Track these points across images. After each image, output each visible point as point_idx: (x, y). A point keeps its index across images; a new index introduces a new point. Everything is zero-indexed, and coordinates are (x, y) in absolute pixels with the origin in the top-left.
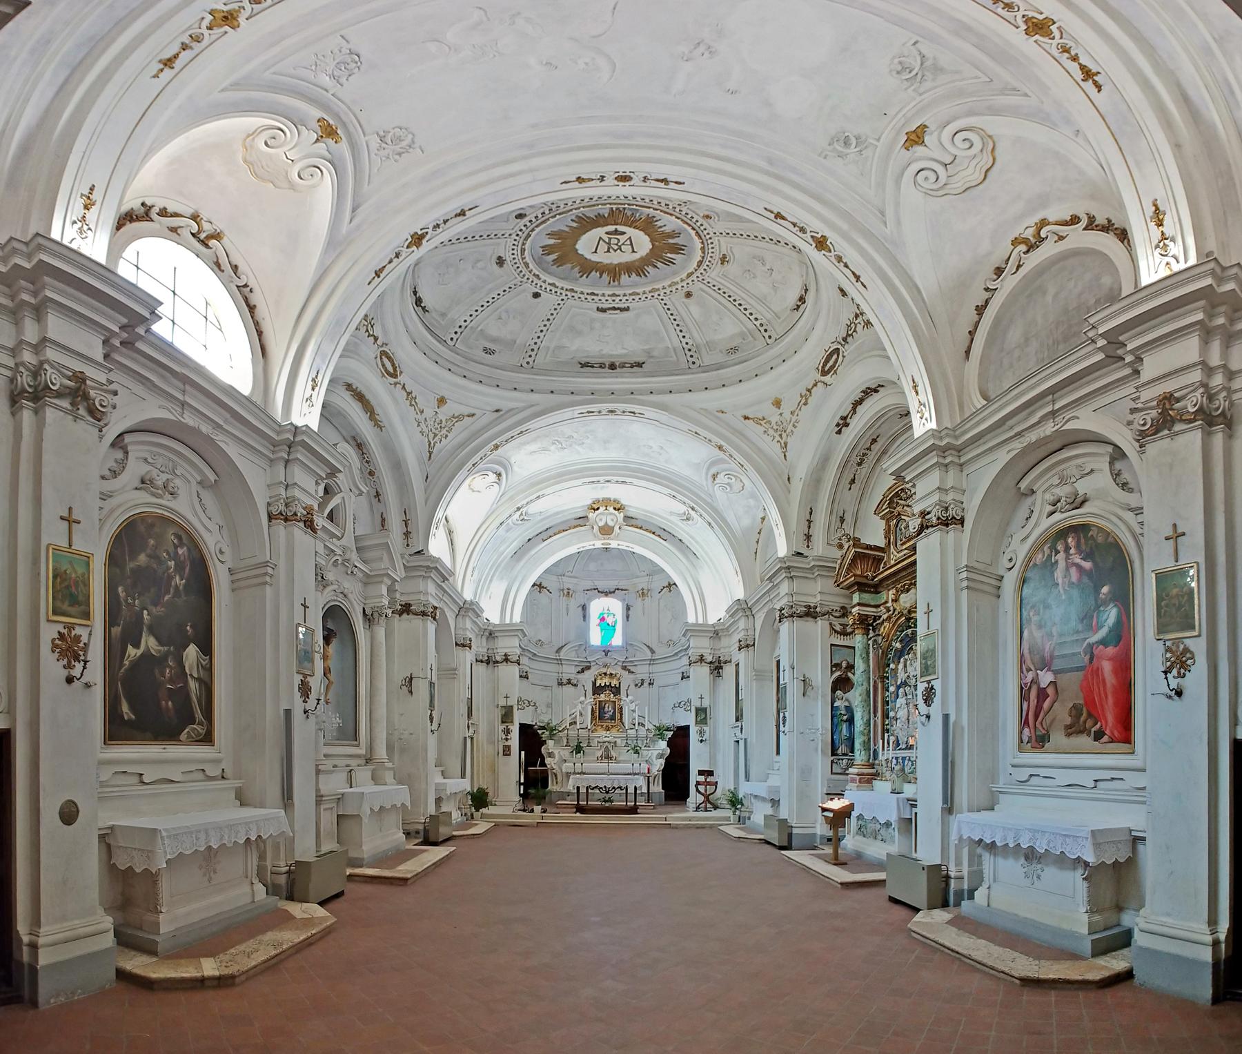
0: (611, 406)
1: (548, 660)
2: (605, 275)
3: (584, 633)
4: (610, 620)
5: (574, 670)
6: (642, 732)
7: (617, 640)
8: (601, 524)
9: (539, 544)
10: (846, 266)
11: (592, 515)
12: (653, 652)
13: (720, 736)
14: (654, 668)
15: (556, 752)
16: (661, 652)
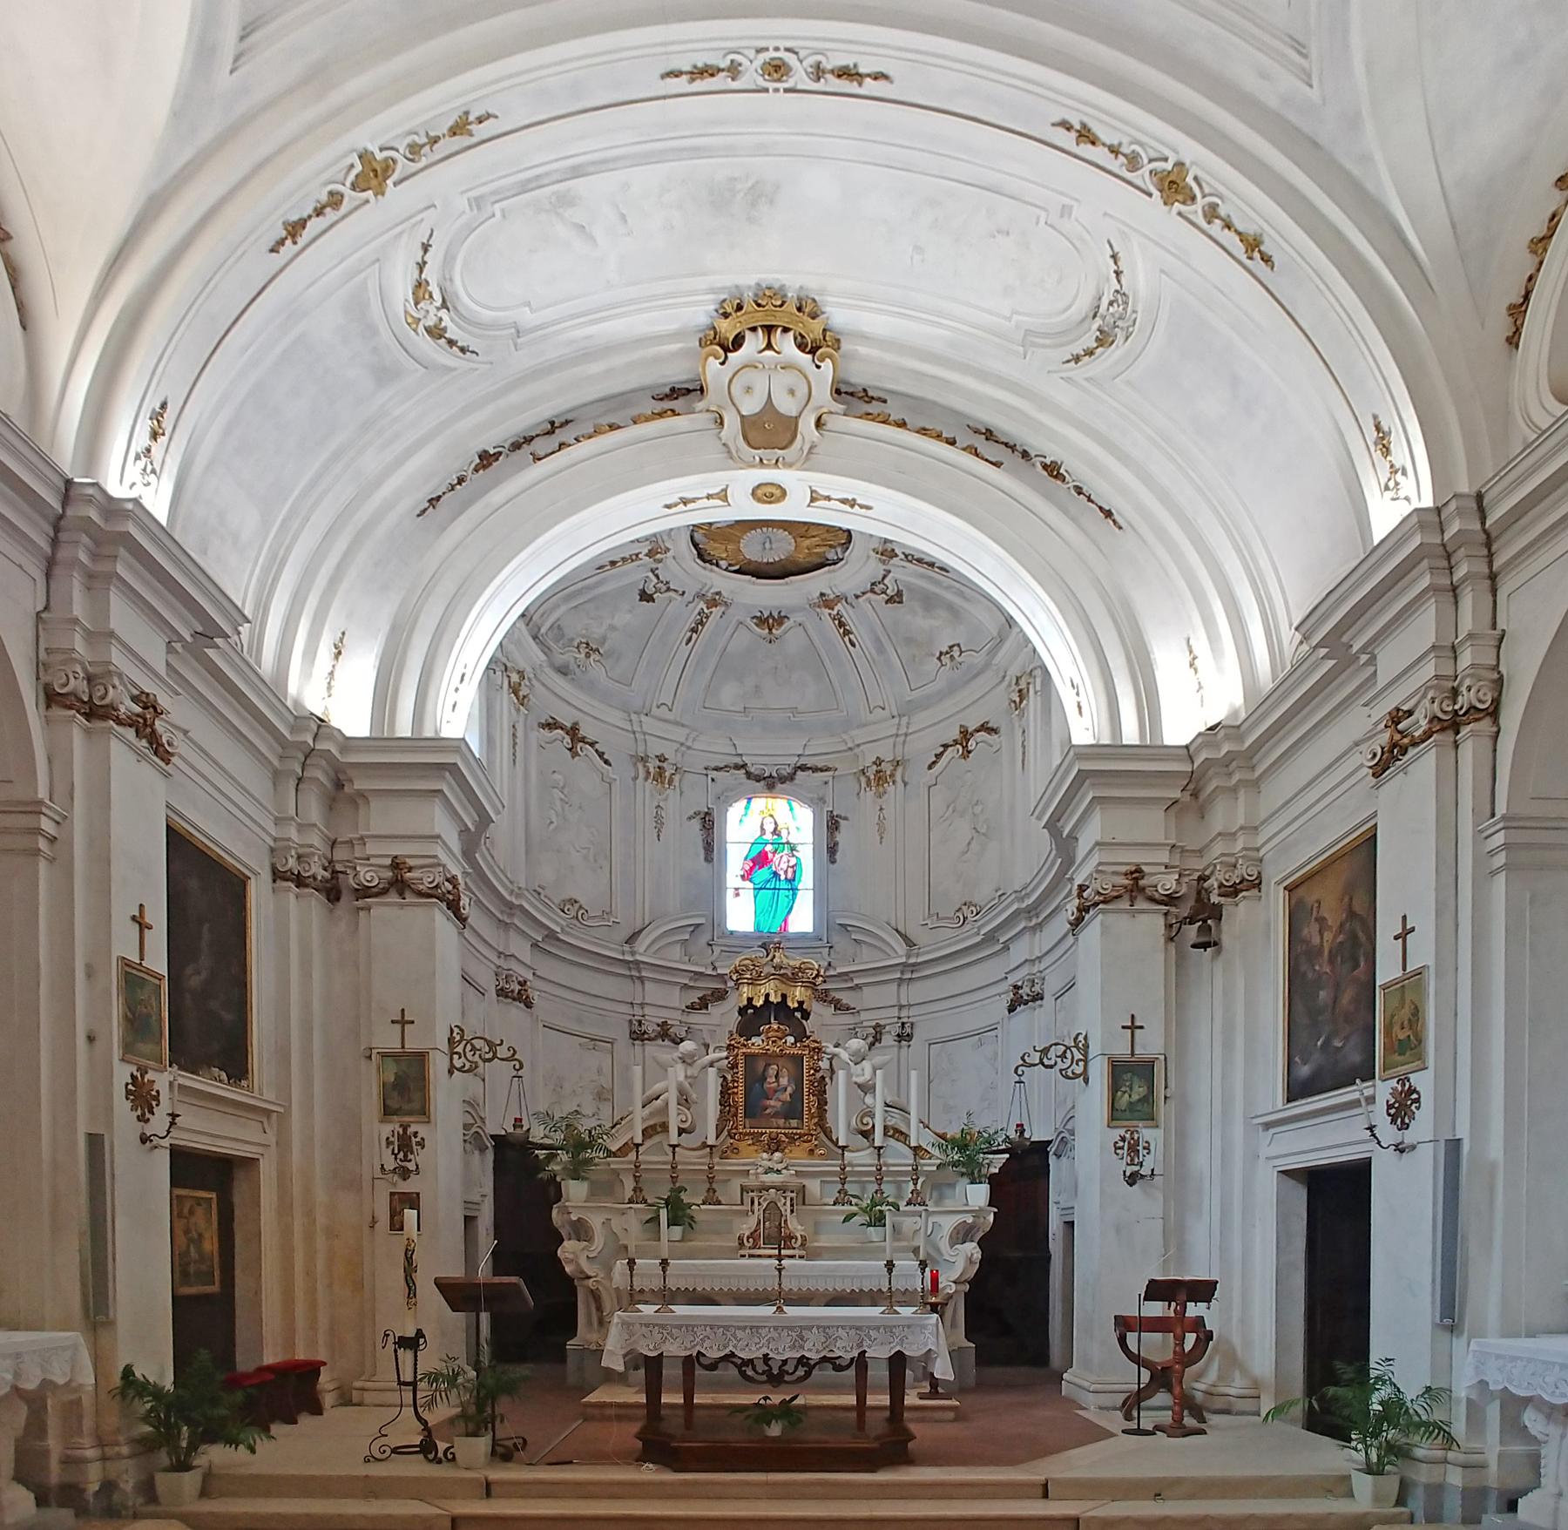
1: (602, 964)
3: (712, 896)
4: (781, 862)
5: (677, 999)
6: (898, 1157)
7: (802, 920)
8: (751, 406)
9: (521, 468)
11: (714, 371)
12: (910, 943)
13: (1201, 1157)
14: (915, 993)
15: (595, 1221)
16: (933, 944)
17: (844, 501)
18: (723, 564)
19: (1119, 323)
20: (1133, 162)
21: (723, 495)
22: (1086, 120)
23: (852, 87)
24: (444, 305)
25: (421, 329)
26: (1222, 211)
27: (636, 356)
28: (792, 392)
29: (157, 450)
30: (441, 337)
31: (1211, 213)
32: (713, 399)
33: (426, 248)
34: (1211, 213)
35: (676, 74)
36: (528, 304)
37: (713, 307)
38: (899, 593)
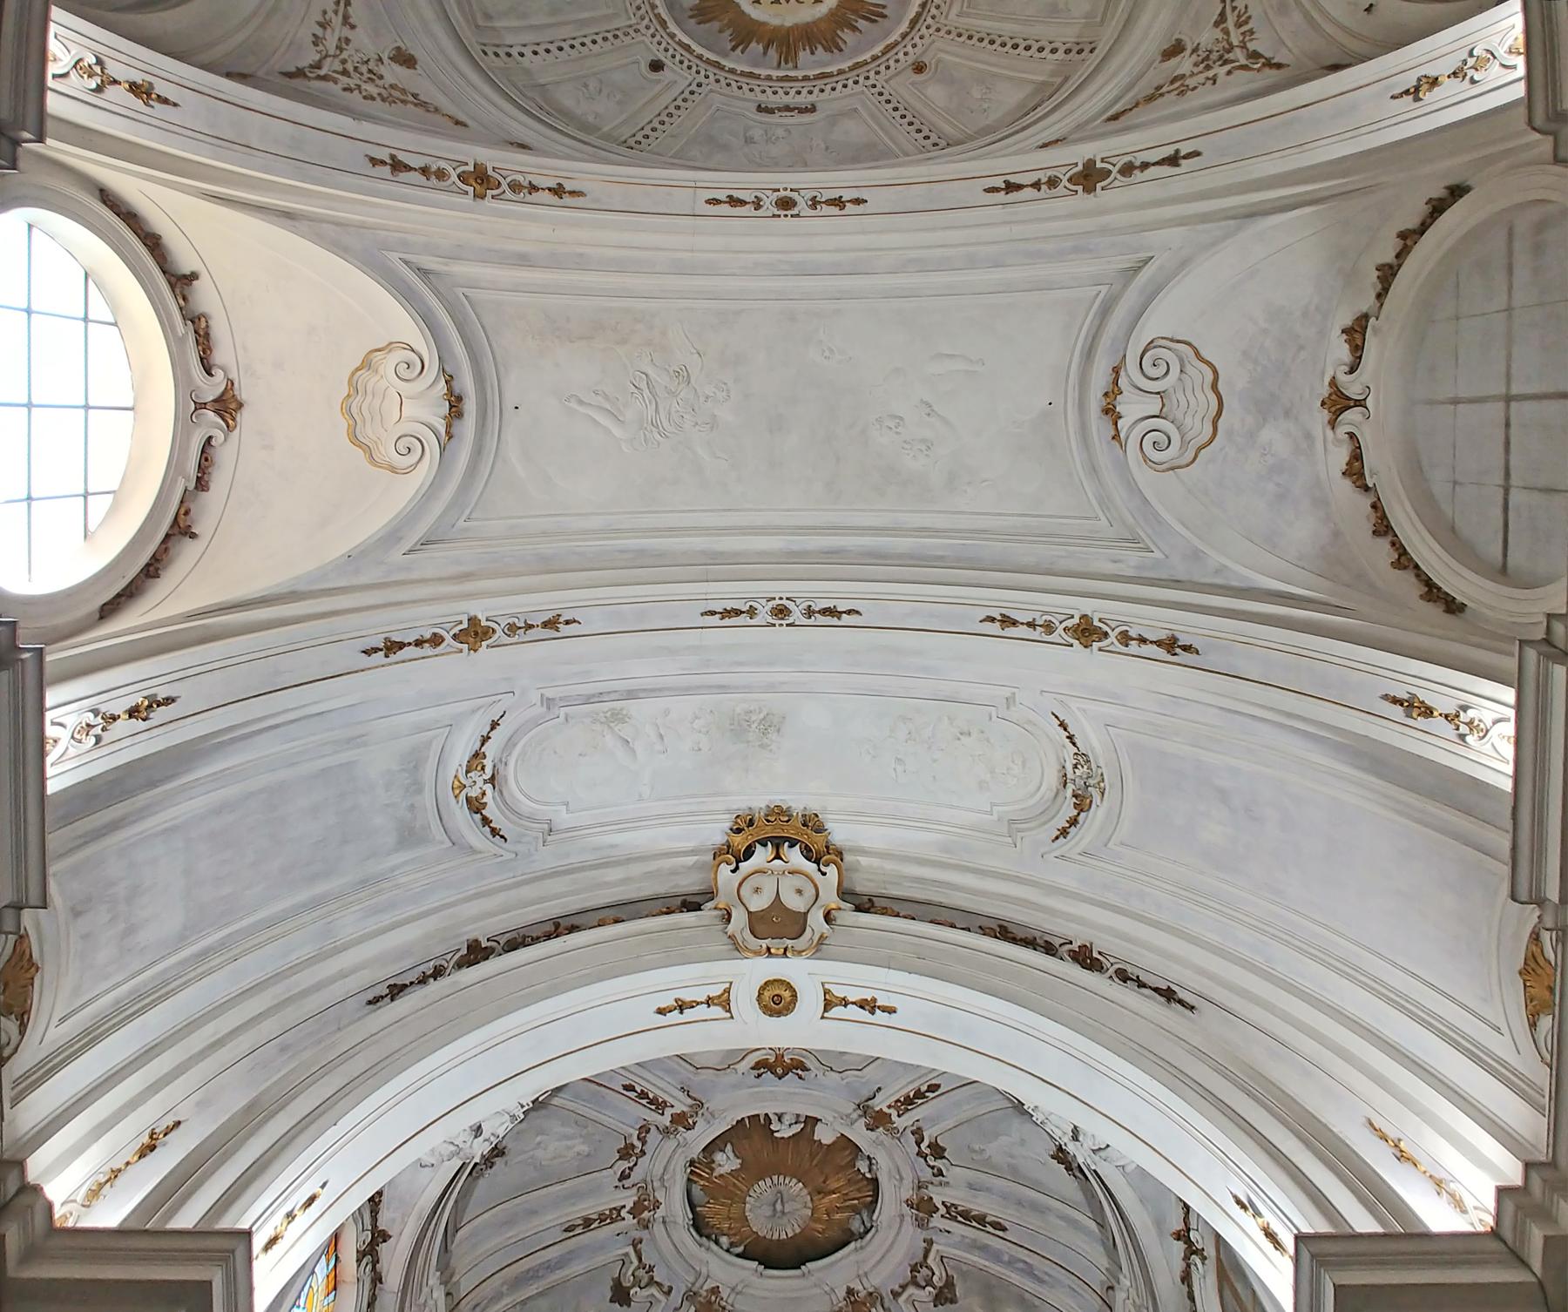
0: (786, 181)
2: (772, 52)
8: (759, 903)
10: (1142, 640)
17: (862, 1004)
18: (724, 1240)
19: (1091, 781)
20: (1049, 628)
21: (723, 1001)
22: (1004, 611)
23: (835, 621)
24: (492, 780)
25: (462, 797)
26: (1133, 633)
27: (653, 866)
28: (799, 892)
29: (124, 726)
30: (478, 811)
31: (1125, 638)
32: (721, 901)
33: (494, 725)
34: (1125, 638)
35: (713, 613)
36: (567, 804)
37: (729, 825)
38: (949, 1283)
